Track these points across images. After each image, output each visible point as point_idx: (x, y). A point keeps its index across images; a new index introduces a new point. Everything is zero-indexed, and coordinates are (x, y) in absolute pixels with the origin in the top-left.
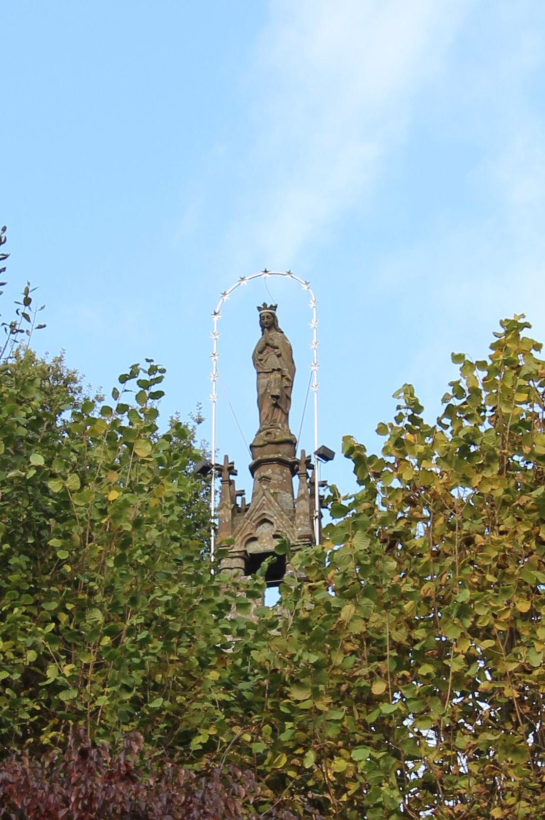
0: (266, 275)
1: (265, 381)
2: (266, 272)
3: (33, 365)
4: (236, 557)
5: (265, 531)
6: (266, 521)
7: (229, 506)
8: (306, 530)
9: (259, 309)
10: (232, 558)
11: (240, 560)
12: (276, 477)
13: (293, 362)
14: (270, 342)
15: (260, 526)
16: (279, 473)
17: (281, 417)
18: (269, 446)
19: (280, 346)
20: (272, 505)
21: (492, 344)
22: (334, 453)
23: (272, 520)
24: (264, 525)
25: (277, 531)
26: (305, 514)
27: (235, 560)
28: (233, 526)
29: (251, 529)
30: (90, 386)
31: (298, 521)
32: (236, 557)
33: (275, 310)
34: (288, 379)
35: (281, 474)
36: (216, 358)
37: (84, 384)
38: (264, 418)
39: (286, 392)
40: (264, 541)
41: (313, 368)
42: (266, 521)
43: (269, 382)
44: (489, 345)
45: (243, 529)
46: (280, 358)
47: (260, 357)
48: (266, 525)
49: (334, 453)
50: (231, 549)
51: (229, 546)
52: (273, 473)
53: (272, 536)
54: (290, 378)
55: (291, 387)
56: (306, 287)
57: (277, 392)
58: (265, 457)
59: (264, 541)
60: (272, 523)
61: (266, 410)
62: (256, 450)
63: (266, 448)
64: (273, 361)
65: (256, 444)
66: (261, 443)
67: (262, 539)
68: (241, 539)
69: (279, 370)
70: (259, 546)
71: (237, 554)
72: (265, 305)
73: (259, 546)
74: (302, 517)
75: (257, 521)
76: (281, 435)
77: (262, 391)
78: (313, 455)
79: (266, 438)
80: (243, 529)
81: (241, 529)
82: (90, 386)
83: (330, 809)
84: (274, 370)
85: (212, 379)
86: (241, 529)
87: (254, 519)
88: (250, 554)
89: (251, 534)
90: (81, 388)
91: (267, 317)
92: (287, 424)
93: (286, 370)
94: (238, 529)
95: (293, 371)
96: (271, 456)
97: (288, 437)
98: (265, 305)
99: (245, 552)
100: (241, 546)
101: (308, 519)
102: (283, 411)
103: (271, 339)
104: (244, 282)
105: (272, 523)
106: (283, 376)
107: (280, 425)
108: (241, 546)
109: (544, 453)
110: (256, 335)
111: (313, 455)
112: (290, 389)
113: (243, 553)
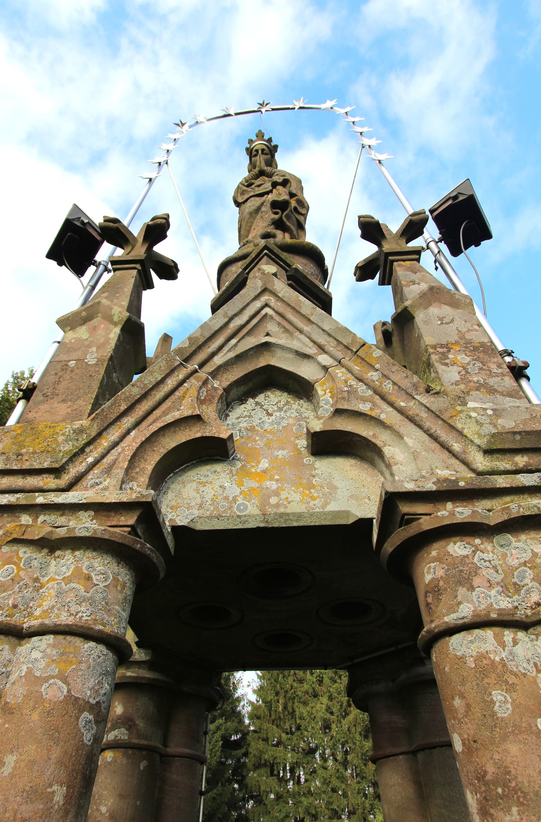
3: (31, 450)
15: (242, 400)
18: (253, 199)
24: (260, 398)
25: (338, 412)
29: (201, 402)
40: (264, 464)
45: (159, 395)
50: (68, 488)
51: (56, 472)
53: (303, 443)
59: (264, 464)
70: (233, 490)
73: (233, 490)
80: (159, 395)
81: (144, 396)
83: (233, 738)
86: (144, 396)
87: (218, 360)
88: (176, 530)
89: (197, 418)
109: (539, 429)
113: (131, 519)
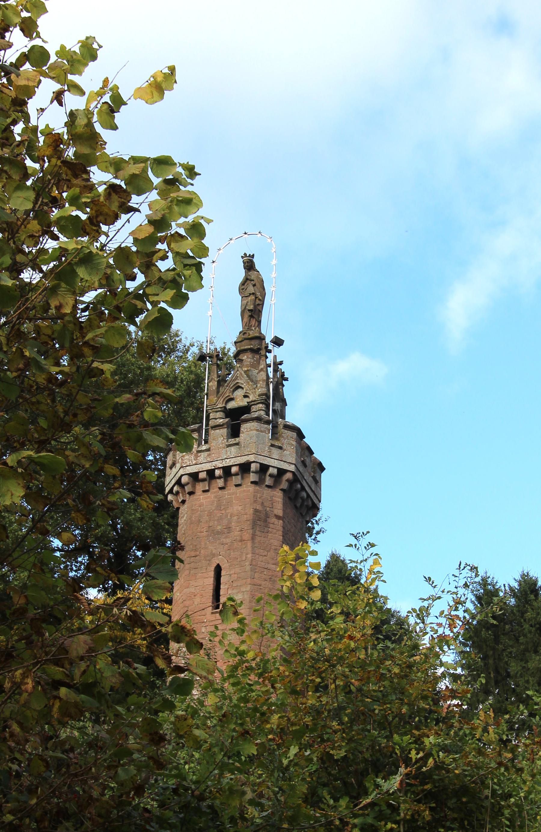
0: (246, 236)
1: (245, 302)
2: (245, 233)
4: (219, 411)
5: (239, 394)
6: (239, 387)
7: (216, 379)
8: (264, 390)
9: (242, 257)
10: (216, 412)
11: (222, 413)
12: (249, 360)
13: (264, 289)
14: (249, 277)
16: (251, 357)
17: (255, 324)
19: (255, 279)
20: (243, 377)
21: (116, 130)
22: (284, 341)
23: (243, 386)
26: (263, 381)
27: (218, 413)
28: (218, 392)
30: (186, 338)
31: (259, 385)
32: (219, 411)
33: (253, 258)
34: (259, 300)
35: (253, 358)
36: (213, 289)
37: (183, 337)
38: (244, 325)
39: (259, 308)
41: (272, 289)
42: (239, 387)
43: (247, 302)
44: (117, 130)
46: (255, 287)
47: (243, 287)
48: (240, 390)
49: (284, 341)
52: (248, 358)
54: (260, 298)
55: (263, 304)
56: (269, 240)
57: (251, 307)
58: (242, 348)
60: (243, 388)
61: (246, 320)
62: (237, 344)
63: (243, 343)
64: (251, 289)
65: (238, 341)
66: (240, 340)
67: (237, 399)
68: (222, 399)
69: (253, 294)
71: (220, 409)
72: (245, 254)
74: (261, 382)
75: (234, 388)
76: (253, 334)
77: (244, 307)
78: (269, 343)
79: (243, 336)
82: (186, 338)
84: (250, 294)
85: (210, 302)
89: (229, 396)
90: (181, 339)
91: (247, 262)
92: (260, 328)
93: (258, 294)
94: (220, 393)
95: (264, 295)
96: (246, 347)
97: (257, 335)
98: (245, 254)
99: (225, 407)
100: (222, 404)
101: (265, 384)
102: (256, 320)
103: (250, 276)
104: (232, 241)
105: (243, 388)
106: (256, 298)
107: (253, 328)
108: (222, 404)
110: (241, 274)
111: (269, 343)
112: (261, 306)
